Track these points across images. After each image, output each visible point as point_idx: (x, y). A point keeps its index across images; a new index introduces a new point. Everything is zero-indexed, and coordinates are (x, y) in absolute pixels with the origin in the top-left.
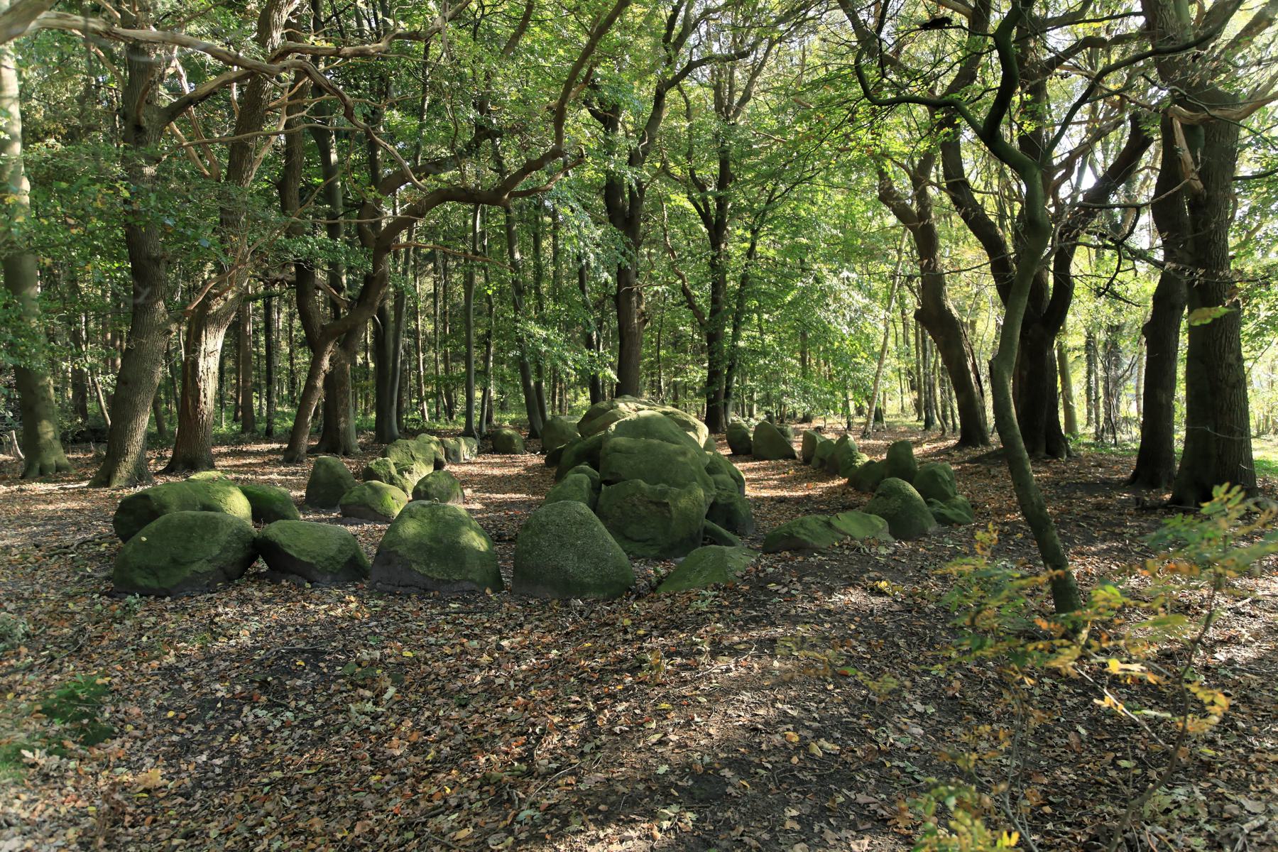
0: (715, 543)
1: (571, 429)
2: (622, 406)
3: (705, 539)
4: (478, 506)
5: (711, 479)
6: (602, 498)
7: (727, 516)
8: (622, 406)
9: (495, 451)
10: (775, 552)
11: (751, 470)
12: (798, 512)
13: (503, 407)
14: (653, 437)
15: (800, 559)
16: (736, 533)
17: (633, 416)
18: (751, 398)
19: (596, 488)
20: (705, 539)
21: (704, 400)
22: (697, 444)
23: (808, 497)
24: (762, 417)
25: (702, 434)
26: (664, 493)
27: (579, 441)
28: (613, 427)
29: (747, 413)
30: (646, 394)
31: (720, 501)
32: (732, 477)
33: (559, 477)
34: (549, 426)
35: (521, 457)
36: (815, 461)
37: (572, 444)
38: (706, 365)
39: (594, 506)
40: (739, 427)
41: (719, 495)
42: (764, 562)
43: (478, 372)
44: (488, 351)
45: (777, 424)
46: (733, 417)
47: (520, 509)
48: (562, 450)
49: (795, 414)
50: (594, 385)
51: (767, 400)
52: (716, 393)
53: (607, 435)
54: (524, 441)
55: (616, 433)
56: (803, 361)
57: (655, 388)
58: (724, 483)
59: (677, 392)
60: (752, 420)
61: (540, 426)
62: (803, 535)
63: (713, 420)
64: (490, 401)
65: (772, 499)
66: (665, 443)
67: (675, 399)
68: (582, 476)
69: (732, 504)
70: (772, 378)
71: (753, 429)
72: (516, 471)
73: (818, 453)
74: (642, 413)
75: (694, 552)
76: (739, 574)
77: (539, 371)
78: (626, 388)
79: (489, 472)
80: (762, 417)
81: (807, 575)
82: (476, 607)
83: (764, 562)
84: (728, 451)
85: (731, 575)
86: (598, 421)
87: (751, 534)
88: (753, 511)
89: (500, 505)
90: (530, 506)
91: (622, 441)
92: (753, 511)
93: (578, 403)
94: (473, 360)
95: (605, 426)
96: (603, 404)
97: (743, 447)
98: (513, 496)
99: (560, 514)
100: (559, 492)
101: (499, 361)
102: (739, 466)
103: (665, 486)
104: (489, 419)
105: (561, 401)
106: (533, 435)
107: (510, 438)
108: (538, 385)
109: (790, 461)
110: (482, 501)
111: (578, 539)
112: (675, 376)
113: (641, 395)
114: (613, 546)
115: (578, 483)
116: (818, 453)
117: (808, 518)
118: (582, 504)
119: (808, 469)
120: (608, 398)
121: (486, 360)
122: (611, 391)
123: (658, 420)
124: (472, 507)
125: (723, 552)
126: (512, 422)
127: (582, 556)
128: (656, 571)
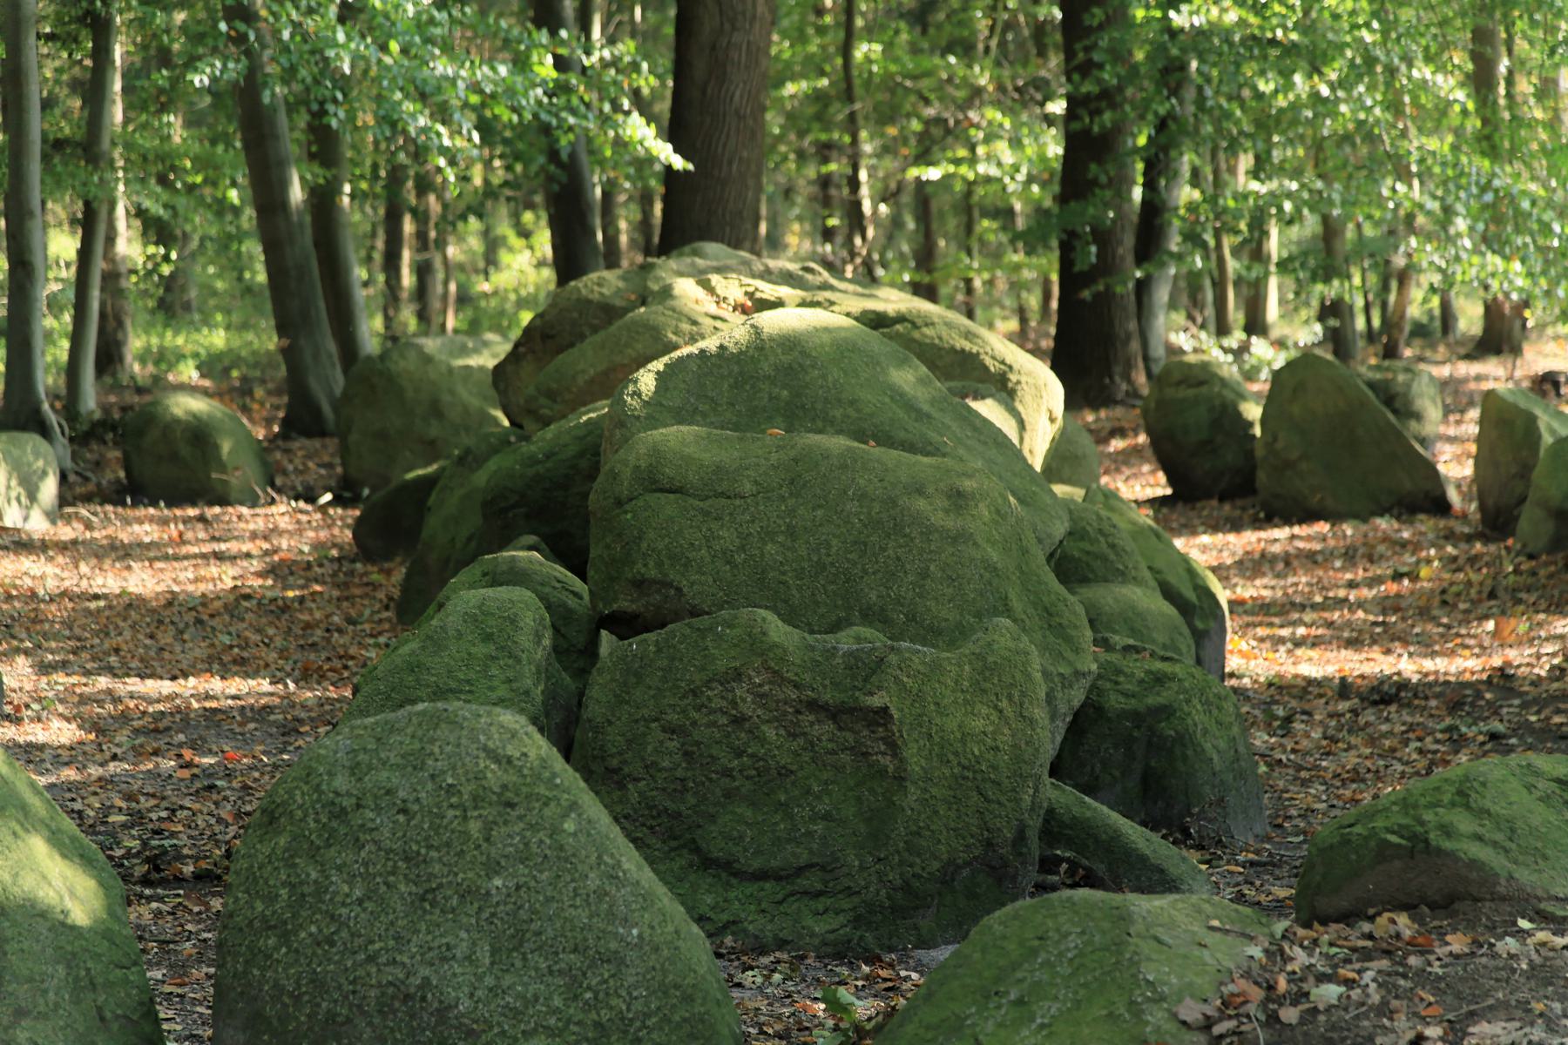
0: (1090, 881)
1: (469, 397)
2: (686, 289)
3: (1048, 864)
4: (61, 732)
5: (1073, 605)
6: (599, 690)
7: (1144, 765)
8: (686, 289)
9: (134, 491)
10: (1348, 917)
11: (1253, 565)
12: (1457, 742)
13: (172, 303)
14: (826, 424)
15: (1458, 943)
16: (1182, 836)
17: (735, 332)
18: (1254, 250)
19: (574, 648)
20: (1048, 864)
21: (1048, 264)
22: (1012, 454)
23: (1503, 679)
24: (1308, 333)
25: (1038, 410)
26: (867, 668)
27: (504, 443)
28: (646, 380)
29: (1236, 315)
30: (796, 239)
31: (1115, 702)
32: (1169, 593)
33: (413, 605)
34: (371, 380)
35: (247, 519)
36: (1531, 522)
37: (469, 461)
38: (1057, 107)
39: (566, 728)
40: (1201, 376)
41: (1110, 673)
42: (1300, 958)
43: (57, 145)
44: (101, 54)
45: (1367, 363)
46: (1181, 336)
47: (246, 741)
48: (429, 483)
49: (1447, 316)
50: (561, 191)
51: (1324, 257)
52: (1103, 237)
53: (621, 421)
54: (262, 452)
55: (661, 409)
56: (1481, 80)
57: (835, 205)
58: (1133, 621)
59: (935, 230)
60: (1260, 348)
61: (329, 381)
62: (1468, 841)
63: (1088, 349)
64: (112, 278)
65: (1344, 688)
66: (873, 450)
67: (925, 257)
68: (512, 596)
69: (1166, 711)
70: (1361, 158)
71: (1261, 385)
72: (225, 577)
73: (1547, 484)
74: (771, 321)
75: (996, 920)
76: (1191, 1011)
77: (324, 146)
78: (698, 213)
79: (108, 581)
80: (1308, 333)
81: (1489, 1014)
82: (1556, 993)
83: (1300, 958)
84: (1156, 485)
85: (1156, 1017)
86: (584, 359)
87: (1247, 836)
88: (1261, 739)
89: (161, 728)
90: (290, 730)
91: (678, 438)
92: (1261, 739)
93: (502, 279)
94: (35, 94)
95: (613, 379)
96: (602, 283)
97: (1216, 468)
98: (216, 685)
99: (414, 762)
100: (413, 667)
101: (146, 102)
102: (1205, 549)
103: (872, 636)
104: (109, 356)
105: (423, 271)
106: (302, 420)
107: (199, 434)
108: (322, 199)
109: (1427, 524)
110: (78, 707)
111: (493, 868)
112: (924, 157)
113: (775, 243)
114: (647, 899)
115: (494, 632)
116: (1547, 484)
117: (1493, 767)
118: (509, 718)
119: (1505, 558)
120: (631, 258)
121: (93, 91)
122: (645, 224)
123: (841, 348)
124: (34, 733)
125: (1122, 918)
126: (211, 365)
127: (513, 941)
128: (837, 1008)
